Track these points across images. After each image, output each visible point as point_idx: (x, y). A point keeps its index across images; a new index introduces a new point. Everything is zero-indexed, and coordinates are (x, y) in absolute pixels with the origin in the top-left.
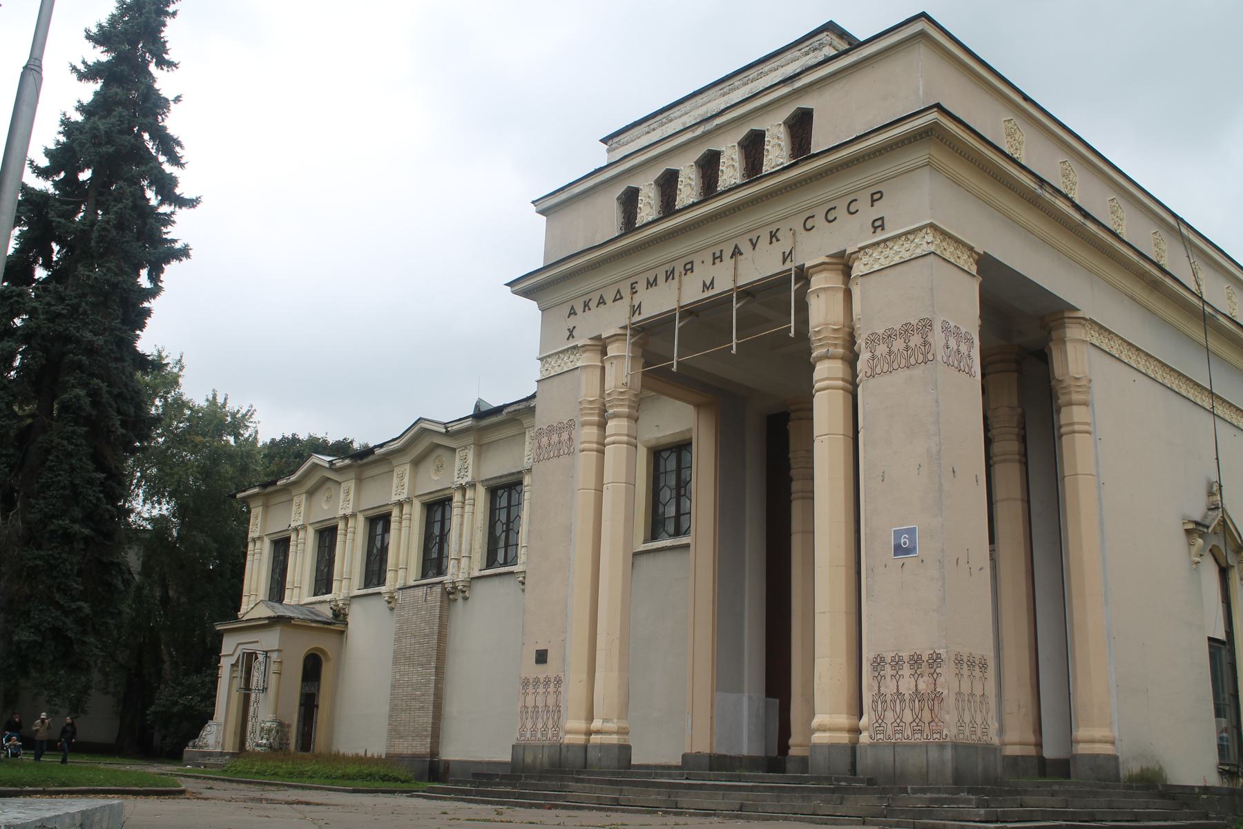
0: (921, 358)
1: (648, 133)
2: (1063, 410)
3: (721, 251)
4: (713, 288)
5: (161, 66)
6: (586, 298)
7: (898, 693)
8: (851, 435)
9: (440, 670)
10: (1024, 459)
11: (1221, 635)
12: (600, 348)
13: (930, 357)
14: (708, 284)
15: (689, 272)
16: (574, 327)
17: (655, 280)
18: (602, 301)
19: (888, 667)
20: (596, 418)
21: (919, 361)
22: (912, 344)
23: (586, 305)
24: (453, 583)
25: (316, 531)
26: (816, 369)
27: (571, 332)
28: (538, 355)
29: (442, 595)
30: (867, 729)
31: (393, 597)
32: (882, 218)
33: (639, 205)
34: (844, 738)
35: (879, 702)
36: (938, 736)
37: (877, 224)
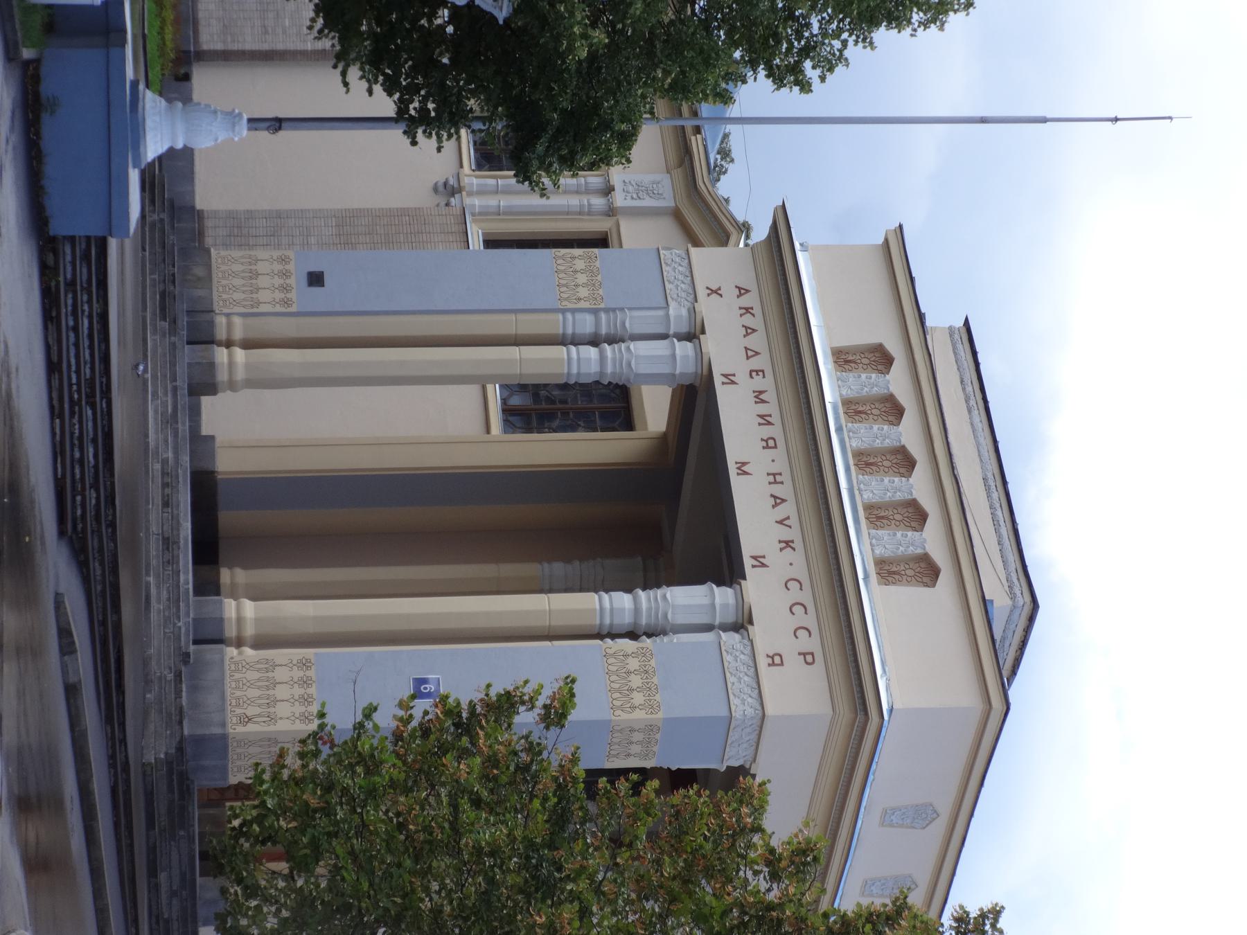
0: (617, 703)
3: (782, 483)
7: (275, 684)
12: (693, 331)
15: (765, 444)
16: (721, 296)
17: (763, 401)
18: (749, 331)
19: (301, 674)
20: (604, 331)
23: (748, 310)
27: (716, 292)
30: (240, 653)
32: (782, 664)
34: (221, 334)
35: (266, 666)
36: (234, 704)
37: (777, 660)
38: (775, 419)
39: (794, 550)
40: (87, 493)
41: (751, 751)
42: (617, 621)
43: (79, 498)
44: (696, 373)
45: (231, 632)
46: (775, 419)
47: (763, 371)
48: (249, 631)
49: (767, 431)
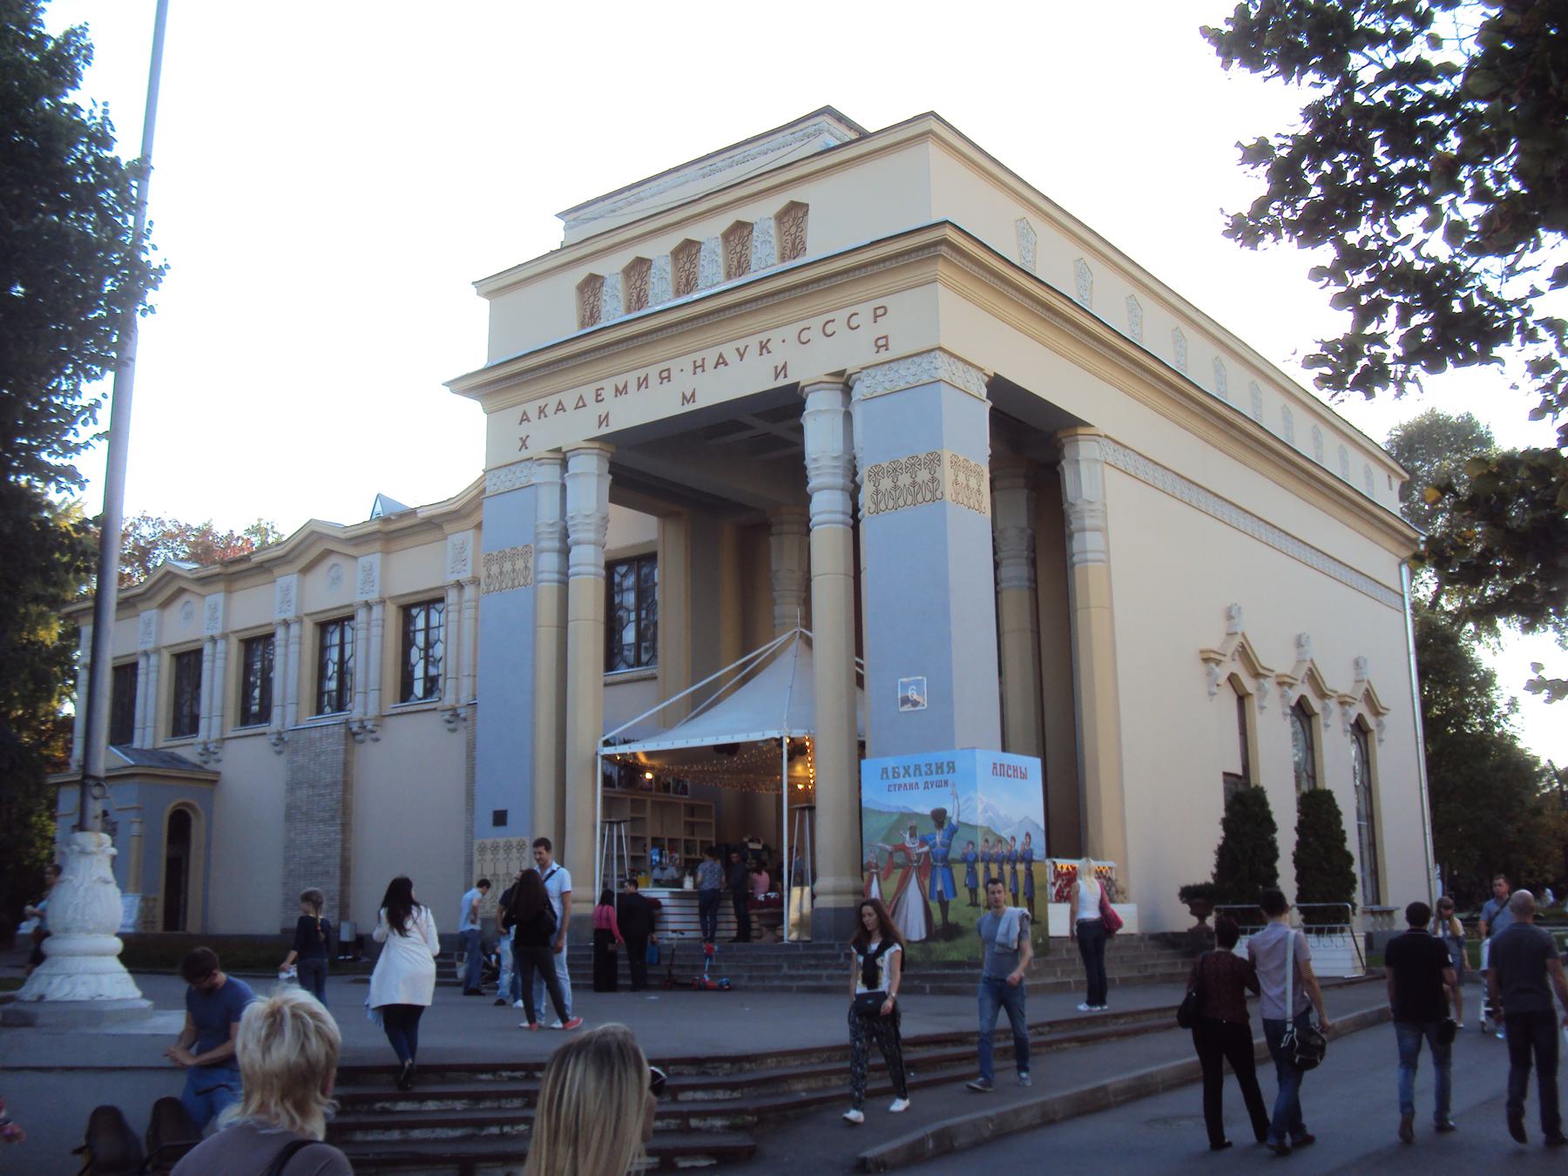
1: (614, 211)
2: (1076, 536)
4: (694, 402)
6: (541, 402)
8: (852, 574)
9: (345, 827)
11: (1238, 770)
12: (559, 461)
13: (938, 494)
17: (625, 387)
18: (560, 407)
21: (927, 498)
22: (919, 480)
24: (362, 721)
25: (173, 655)
31: (282, 739)
32: (885, 337)
33: (605, 298)
38: (641, 373)
40: (685, 1108)
41: (973, 372)
43: (694, 1122)
44: (598, 455)
45: (849, 901)
46: (641, 373)
48: (848, 882)
49: (654, 379)
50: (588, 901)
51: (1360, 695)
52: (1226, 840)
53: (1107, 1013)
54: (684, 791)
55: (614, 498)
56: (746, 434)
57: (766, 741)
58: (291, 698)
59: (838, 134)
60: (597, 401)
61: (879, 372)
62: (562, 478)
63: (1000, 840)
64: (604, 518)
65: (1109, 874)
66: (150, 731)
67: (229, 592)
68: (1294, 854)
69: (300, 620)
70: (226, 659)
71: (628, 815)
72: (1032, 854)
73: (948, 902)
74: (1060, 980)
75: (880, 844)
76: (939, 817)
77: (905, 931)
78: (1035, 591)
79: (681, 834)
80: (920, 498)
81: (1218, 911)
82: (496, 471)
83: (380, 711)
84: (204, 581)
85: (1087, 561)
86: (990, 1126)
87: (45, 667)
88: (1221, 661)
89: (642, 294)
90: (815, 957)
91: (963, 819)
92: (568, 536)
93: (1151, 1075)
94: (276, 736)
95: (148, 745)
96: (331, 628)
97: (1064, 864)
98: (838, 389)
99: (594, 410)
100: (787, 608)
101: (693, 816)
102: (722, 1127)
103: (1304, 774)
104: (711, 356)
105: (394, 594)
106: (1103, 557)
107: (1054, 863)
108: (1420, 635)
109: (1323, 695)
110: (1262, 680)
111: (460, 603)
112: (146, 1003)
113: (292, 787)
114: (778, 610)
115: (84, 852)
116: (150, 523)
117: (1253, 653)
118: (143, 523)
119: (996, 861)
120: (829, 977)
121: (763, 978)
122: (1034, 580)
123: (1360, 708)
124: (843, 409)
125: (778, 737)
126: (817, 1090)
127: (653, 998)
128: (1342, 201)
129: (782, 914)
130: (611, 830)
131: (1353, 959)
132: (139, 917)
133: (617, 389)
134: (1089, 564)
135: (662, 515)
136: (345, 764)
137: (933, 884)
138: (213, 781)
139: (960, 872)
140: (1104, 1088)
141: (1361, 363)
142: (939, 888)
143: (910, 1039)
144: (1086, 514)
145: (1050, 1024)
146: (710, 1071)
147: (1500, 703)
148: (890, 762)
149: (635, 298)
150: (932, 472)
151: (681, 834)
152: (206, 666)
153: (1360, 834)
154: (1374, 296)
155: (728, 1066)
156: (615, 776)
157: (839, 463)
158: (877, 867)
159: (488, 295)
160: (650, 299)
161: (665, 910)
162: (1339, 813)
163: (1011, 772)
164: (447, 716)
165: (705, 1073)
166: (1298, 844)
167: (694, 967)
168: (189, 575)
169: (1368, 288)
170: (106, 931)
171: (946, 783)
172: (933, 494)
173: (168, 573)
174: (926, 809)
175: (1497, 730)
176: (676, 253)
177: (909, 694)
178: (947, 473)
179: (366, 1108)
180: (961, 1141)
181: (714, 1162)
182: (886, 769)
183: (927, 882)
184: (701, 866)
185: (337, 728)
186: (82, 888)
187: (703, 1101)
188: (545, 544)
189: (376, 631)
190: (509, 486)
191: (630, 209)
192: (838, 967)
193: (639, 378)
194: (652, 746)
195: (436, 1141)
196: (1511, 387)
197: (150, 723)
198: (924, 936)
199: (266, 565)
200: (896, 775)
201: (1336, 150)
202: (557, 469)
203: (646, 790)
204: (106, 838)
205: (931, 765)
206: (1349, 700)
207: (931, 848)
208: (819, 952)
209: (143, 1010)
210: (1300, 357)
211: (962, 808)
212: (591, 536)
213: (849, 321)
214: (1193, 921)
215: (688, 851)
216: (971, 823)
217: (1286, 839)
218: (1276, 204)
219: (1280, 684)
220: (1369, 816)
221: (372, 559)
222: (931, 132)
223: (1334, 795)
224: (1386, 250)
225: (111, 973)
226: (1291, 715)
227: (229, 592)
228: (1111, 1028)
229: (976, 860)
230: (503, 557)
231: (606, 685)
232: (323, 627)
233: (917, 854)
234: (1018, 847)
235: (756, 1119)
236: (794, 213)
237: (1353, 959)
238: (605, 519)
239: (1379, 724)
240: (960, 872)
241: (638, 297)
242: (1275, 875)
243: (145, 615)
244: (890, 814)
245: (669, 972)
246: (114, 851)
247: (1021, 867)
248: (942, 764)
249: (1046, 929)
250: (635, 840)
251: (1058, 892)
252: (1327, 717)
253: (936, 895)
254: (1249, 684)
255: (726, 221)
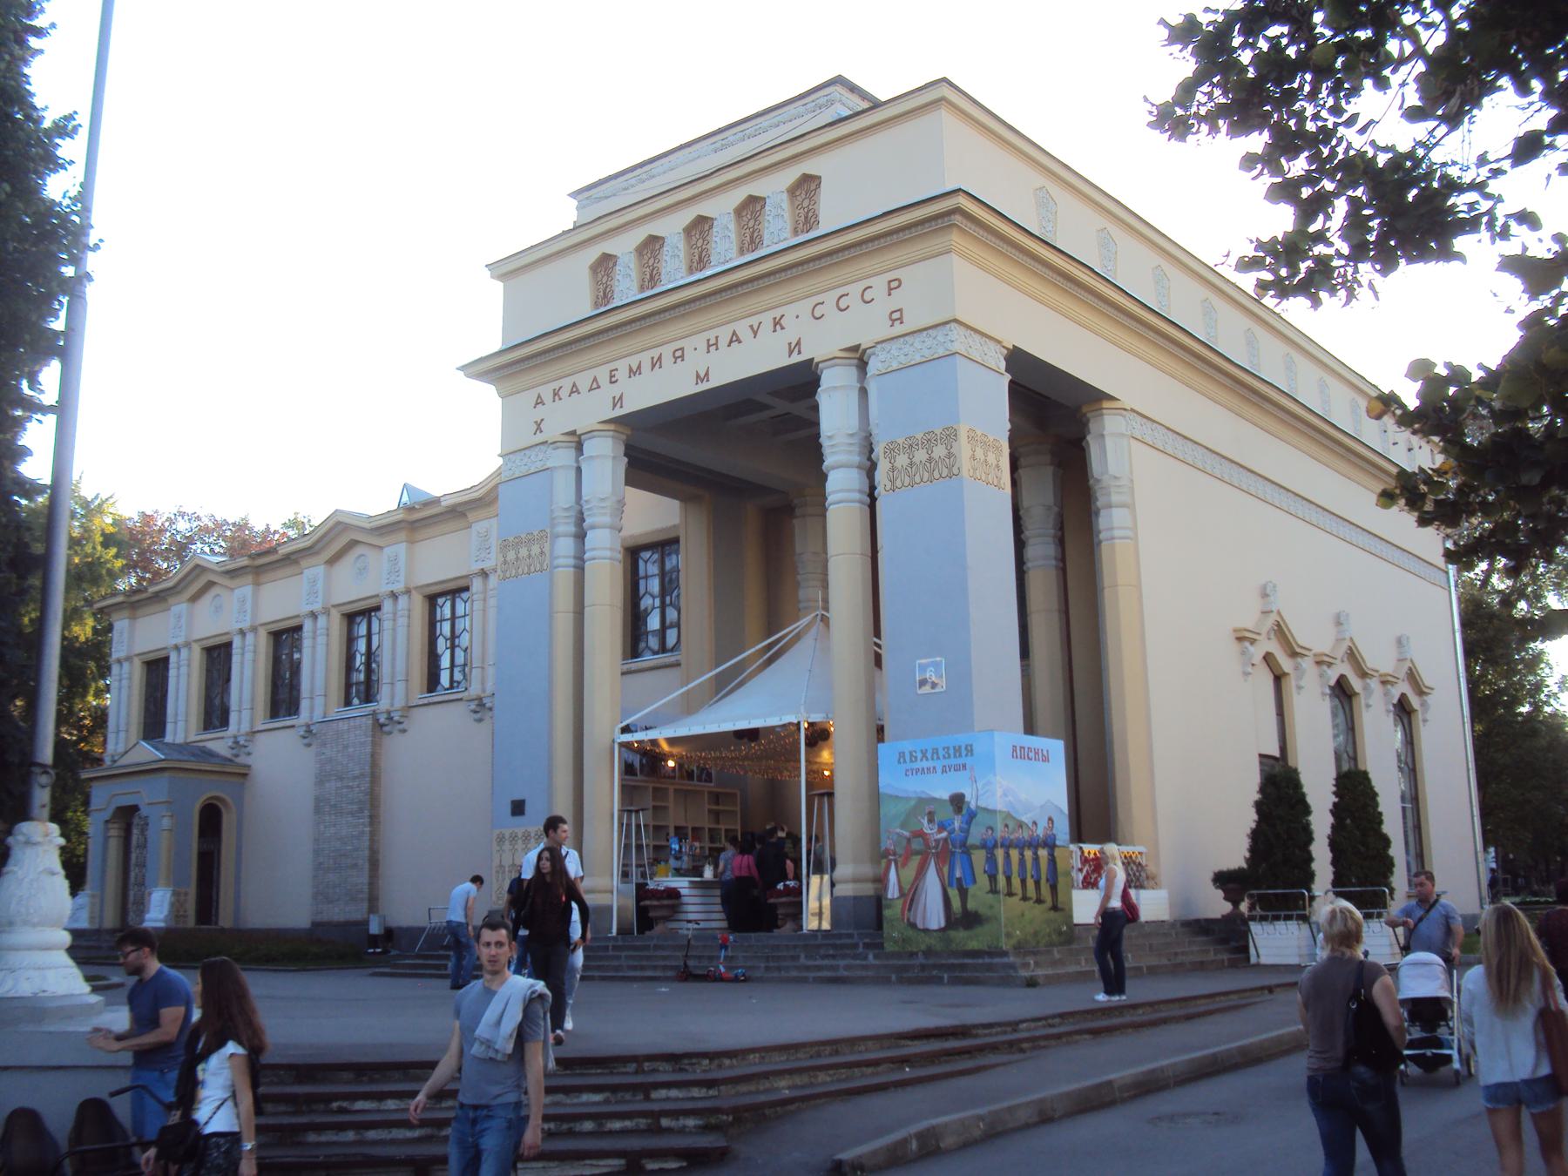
1: (626, 189)
2: (1103, 513)
3: (717, 337)
4: (708, 380)
5: (49, 133)
6: (555, 385)
9: (374, 819)
10: (1061, 565)
11: (1276, 753)
12: (574, 444)
13: (955, 471)
14: (702, 376)
17: (639, 367)
18: (575, 390)
22: (935, 455)
24: (389, 712)
26: (829, 478)
28: (499, 452)
29: (373, 725)
32: (900, 310)
33: (618, 277)
37: (896, 316)
38: (655, 353)
39: (783, 316)
40: (656, 1107)
41: (992, 345)
42: (856, 485)
43: (665, 1122)
44: (613, 437)
45: (868, 889)
46: (655, 353)
47: (611, 371)
48: (867, 870)
49: (667, 359)
50: (605, 892)
51: (1402, 674)
52: (1259, 823)
53: (1124, 1003)
54: (709, 778)
55: (631, 481)
56: (766, 414)
57: (784, 726)
58: (319, 690)
59: (851, 104)
60: (611, 382)
61: (894, 345)
62: (577, 461)
63: (1021, 825)
64: (619, 501)
65: (1139, 859)
66: (181, 725)
67: (257, 584)
68: (1329, 838)
69: (327, 612)
70: (255, 652)
71: (650, 803)
72: (1055, 839)
73: (967, 889)
74: (1084, 969)
75: (898, 830)
76: (958, 801)
77: (924, 918)
78: (1063, 570)
79: (706, 823)
80: (936, 475)
81: (1251, 896)
82: (511, 456)
83: (407, 701)
84: (232, 573)
85: (1113, 538)
86: (981, 1125)
87: (80, 663)
88: (1255, 640)
89: (655, 272)
90: (835, 946)
91: (982, 804)
92: (583, 520)
93: (1162, 1069)
94: (304, 728)
95: (180, 739)
96: (358, 619)
97: (1091, 849)
98: (850, 365)
99: (608, 392)
100: (808, 592)
101: (718, 804)
102: (695, 1127)
103: (1345, 756)
104: (724, 334)
105: (420, 584)
106: (1129, 533)
107: (1081, 848)
108: (1466, 613)
109: (1363, 674)
110: (1299, 660)
111: (485, 591)
112: (95, 999)
113: (321, 780)
114: (802, 594)
115: (29, 843)
116: (186, 518)
117: (1290, 631)
118: (180, 518)
119: (1016, 846)
120: (847, 968)
121: (779, 969)
122: (1062, 559)
123: (1404, 687)
124: (859, 385)
125: (796, 721)
126: (803, 1087)
127: (663, 989)
128: (1273, 76)
129: (801, 903)
130: (629, 818)
131: (1391, 945)
132: (170, 912)
133: (631, 370)
134: (1117, 541)
135: (684, 499)
136: (372, 756)
137: (951, 870)
138: (243, 774)
139: (979, 857)
140: (1110, 1083)
141: (1304, 266)
142: (958, 874)
143: (908, 1033)
144: (1112, 490)
145: (1062, 1016)
146: (687, 1067)
147: (1549, 681)
148: (906, 746)
149: (648, 276)
150: (949, 448)
151: (706, 823)
152: (236, 659)
153: (1404, 817)
154: (1316, 189)
155: (706, 1062)
156: (637, 765)
157: (855, 440)
158: (895, 854)
159: (503, 277)
160: (663, 277)
161: (685, 900)
162: (1376, 794)
163: (1032, 755)
164: (473, 706)
165: (681, 1070)
166: (1333, 827)
167: (711, 958)
168: (216, 568)
169: (1308, 179)
170: (53, 924)
171: (964, 766)
172: (950, 470)
173: (197, 566)
174: (945, 795)
175: (1547, 709)
176: (689, 231)
177: (928, 676)
178: (964, 448)
179: (322, 1106)
180: (948, 1141)
181: (685, 1164)
182: (904, 753)
183: (946, 869)
184: (723, 856)
185: (364, 719)
186: (26, 880)
187: (677, 1099)
188: (561, 529)
189: (402, 621)
190: (524, 470)
191: (642, 186)
192: (855, 957)
193: (653, 358)
194: (682, 730)
195: (393, 1142)
196: (1506, 312)
197: (181, 717)
198: (943, 924)
199: (293, 557)
200: (913, 758)
201: (1267, 20)
202: (572, 453)
203: (669, 777)
204: (54, 828)
205: (948, 748)
206: (1390, 679)
207: (950, 833)
208: (838, 942)
209: (91, 1006)
210: (1233, 261)
211: (980, 792)
212: (607, 519)
213: (862, 295)
214: (1227, 907)
215: (712, 840)
216: (990, 807)
217: (1321, 822)
218: (1205, 88)
219: (1319, 663)
220: (1413, 800)
221: (397, 549)
222: (943, 99)
223: (1371, 776)
224: (1326, 134)
225: (56, 968)
226: (1330, 696)
227: (257, 584)
228: (1128, 1018)
229: (995, 846)
230: (518, 543)
231: (623, 674)
232: (351, 618)
233: (935, 840)
234: (1040, 832)
235: (731, 1118)
236: (808, 183)
237: (1391, 945)
238: (621, 503)
239: (1423, 704)
240: (979, 857)
241: (651, 275)
242: (1310, 859)
243: (175, 609)
244: (907, 799)
245: (685, 964)
246: (62, 841)
247: (1043, 853)
248: (960, 747)
249: (1071, 917)
250: (658, 829)
251: (1085, 878)
252: (1300, 678)
253: (955, 881)
254: (1286, 664)
255: (738, 195)
